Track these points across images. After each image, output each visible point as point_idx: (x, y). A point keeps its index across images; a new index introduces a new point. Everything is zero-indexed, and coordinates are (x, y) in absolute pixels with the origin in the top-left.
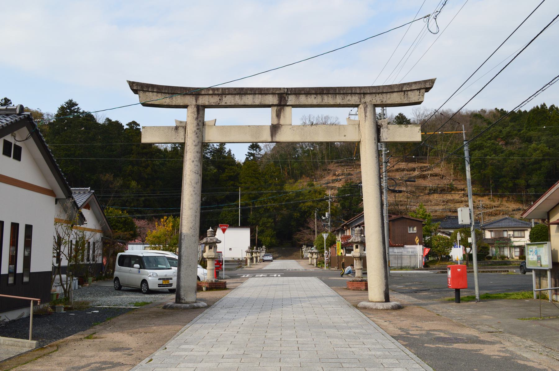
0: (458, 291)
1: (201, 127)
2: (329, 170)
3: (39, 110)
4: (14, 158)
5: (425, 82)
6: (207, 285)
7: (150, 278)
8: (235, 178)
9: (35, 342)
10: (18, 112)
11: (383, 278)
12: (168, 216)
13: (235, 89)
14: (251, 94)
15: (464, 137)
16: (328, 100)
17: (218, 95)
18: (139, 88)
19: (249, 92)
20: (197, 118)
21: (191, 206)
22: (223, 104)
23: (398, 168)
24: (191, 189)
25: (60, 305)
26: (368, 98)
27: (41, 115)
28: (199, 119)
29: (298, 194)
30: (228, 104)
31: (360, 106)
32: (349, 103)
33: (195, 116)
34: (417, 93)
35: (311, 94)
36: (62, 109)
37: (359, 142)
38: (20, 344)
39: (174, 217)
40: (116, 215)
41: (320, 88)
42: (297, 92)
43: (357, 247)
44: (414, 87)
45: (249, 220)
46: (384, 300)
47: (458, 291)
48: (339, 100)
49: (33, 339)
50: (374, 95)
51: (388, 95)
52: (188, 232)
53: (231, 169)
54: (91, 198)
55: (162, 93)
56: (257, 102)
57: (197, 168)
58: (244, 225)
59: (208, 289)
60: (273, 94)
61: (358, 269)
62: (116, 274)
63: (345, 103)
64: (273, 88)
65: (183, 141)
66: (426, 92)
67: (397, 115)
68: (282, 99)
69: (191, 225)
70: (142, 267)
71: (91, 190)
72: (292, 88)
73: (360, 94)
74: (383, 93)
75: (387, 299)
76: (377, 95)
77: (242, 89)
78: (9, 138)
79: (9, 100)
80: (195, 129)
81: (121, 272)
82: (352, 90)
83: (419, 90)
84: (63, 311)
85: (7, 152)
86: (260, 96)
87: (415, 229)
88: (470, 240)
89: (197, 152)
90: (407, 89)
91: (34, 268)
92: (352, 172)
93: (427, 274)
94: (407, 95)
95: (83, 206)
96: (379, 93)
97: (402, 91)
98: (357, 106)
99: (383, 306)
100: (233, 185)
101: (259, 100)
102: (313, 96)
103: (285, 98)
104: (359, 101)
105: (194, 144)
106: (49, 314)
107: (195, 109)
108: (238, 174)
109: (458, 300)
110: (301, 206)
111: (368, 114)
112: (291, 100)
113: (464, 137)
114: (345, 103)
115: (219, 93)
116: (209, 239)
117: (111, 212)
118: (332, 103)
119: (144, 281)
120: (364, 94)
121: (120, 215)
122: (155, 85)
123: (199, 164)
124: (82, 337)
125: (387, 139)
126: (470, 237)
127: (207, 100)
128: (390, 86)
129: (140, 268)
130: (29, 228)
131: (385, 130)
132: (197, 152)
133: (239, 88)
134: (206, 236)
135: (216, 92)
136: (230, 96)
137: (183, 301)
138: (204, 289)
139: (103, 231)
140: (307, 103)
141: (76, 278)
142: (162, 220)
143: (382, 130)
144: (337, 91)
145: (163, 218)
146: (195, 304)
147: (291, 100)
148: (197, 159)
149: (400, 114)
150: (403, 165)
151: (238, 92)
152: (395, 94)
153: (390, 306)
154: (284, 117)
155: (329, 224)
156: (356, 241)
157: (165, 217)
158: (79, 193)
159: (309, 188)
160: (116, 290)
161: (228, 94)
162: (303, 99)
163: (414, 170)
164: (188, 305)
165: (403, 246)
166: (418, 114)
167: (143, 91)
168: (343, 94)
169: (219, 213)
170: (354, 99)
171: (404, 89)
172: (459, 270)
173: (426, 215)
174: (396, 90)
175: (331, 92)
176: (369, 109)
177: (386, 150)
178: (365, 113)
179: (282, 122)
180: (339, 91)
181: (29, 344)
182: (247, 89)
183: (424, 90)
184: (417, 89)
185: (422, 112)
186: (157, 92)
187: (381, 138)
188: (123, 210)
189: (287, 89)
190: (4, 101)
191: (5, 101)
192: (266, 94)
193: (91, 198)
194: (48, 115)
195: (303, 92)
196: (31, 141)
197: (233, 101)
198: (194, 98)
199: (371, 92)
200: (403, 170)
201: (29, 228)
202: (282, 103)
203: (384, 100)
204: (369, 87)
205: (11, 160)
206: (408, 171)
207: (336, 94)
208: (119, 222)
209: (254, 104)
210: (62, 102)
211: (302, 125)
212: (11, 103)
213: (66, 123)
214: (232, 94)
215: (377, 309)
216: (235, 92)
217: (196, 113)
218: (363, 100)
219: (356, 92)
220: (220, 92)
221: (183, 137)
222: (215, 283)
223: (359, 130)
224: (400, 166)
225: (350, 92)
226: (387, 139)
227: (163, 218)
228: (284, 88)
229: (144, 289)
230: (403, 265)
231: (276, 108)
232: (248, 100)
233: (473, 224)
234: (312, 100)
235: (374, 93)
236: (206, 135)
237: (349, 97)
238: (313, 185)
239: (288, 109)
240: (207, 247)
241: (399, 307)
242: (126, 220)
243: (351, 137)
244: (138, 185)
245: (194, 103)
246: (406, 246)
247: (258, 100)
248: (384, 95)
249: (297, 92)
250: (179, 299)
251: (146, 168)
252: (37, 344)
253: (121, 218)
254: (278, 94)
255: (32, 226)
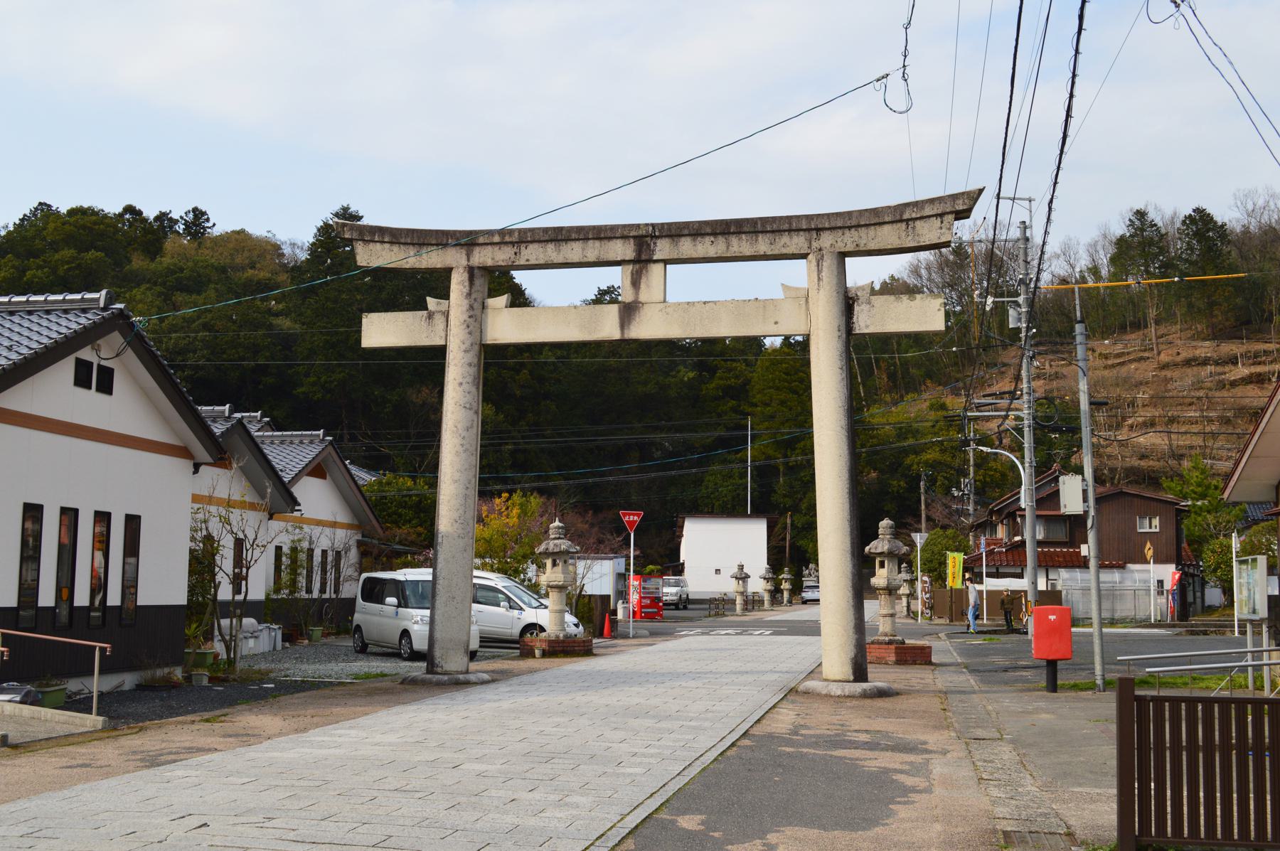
0: (1052, 665)
1: (478, 312)
2: (1005, 365)
3: (270, 235)
4: (98, 390)
5: (954, 197)
6: (545, 646)
7: (416, 627)
8: (739, 392)
9: (101, 718)
10: (102, 305)
11: (851, 631)
12: (511, 492)
13: (546, 230)
14: (578, 240)
15: (1078, 314)
16: (740, 245)
17: (513, 243)
18: (355, 235)
19: (574, 236)
20: (469, 295)
21: (457, 476)
22: (522, 262)
23: (1191, 356)
24: (457, 441)
25: (201, 671)
26: (827, 240)
27: (276, 248)
28: (473, 296)
29: (904, 431)
30: (533, 262)
31: (810, 257)
32: (784, 251)
33: (466, 290)
34: (936, 222)
35: (703, 235)
36: (325, 229)
37: (807, 338)
38: (78, 721)
39: (524, 495)
40: (399, 490)
41: (722, 221)
42: (673, 232)
43: (882, 565)
44: (928, 211)
45: (774, 498)
46: (852, 678)
47: (1052, 665)
48: (763, 245)
49: (99, 714)
50: (840, 232)
51: (872, 231)
52: (450, 530)
53: (730, 370)
54: (324, 454)
55: (399, 243)
56: (591, 257)
57: (469, 398)
58: (757, 513)
59: (545, 654)
60: (624, 237)
61: (885, 616)
62: (358, 618)
63: (777, 250)
64: (624, 226)
65: (442, 343)
66: (956, 219)
67: (1189, 211)
68: (645, 245)
69: (456, 515)
70: (403, 603)
71: (325, 435)
72: (663, 224)
73: (809, 230)
74: (859, 226)
75: (860, 673)
76: (847, 231)
77: (560, 229)
78: (86, 354)
79: (204, 213)
80: (465, 317)
81: (368, 615)
82: (790, 224)
83: (941, 215)
84: (205, 682)
85: (82, 380)
86: (597, 243)
87: (1156, 522)
88: (1084, 550)
89: (470, 365)
90: (914, 215)
91: (146, 597)
92: (1065, 371)
93: (1159, 635)
94: (914, 228)
95: (306, 471)
96: (850, 228)
97: (901, 221)
98: (804, 256)
99: (843, 690)
100: (735, 410)
101: (596, 252)
102: (708, 239)
103: (649, 245)
104: (806, 245)
105: (463, 347)
106: (174, 687)
107: (466, 275)
108: (747, 382)
109: (1053, 687)
110: (908, 461)
111: (825, 274)
112: (663, 249)
113: (1078, 314)
114: (776, 252)
115: (514, 239)
116: (552, 544)
117: (389, 483)
118: (748, 254)
119: (405, 633)
120: (819, 230)
121: (409, 489)
122: (387, 229)
123: (474, 390)
124: (198, 718)
125: (867, 327)
126: (1086, 542)
127: (490, 255)
128: (875, 211)
129: (399, 606)
130: (133, 522)
131: (865, 307)
132: (470, 365)
133: (554, 229)
134: (548, 538)
135: (507, 239)
136: (536, 246)
137: (439, 670)
138: (537, 653)
139: (359, 525)
140: (695, 255)
141: (276, 627)
142: (497, 501)
143: (856, 308)
144: (759, 227)
145: (500, 497)
146: (461, 677)
147: (663, 249)
148: (469, 379)
149: (1197, 210)
150: (1205, 349)
151: (553, 236)
152: (886, 228)
153: (859, 690)
154: (648, 286)
155: (971, 508)
156: (879, 550)
157: (505, 495)
158: (301, 442)
159: (932, 415)
160: (357, 652)
161: (532, 242)
162: (687, 247)
163: (1233, 361)
164: (446, 678)
165: (1122, 567)
166: (1250, 207)
167: (364, 240)
168: (773, 232)
169: (698, 482)
170: (797, 242)
171: (906, 216)
172: (1052, 617)
173: (1208, 487)
174: (887, 219)
175: (746, 229)
176: (829, 263)
177: (1028, 329)
178: (819, 271)
179: (642, 298)
180: (763, 225)
181: (93, 721)
182: (571, 229)
183: (951, 217)
184: (936, 216)
185: (1261, 202)
186: (391, 243)
187: (856, 326)
188: (414, 478)
189: (653, 225)
190: (191, 215)
191: (195, 216)
192: (610, 238)
193: (324, 454)
194: (293, 245)
195: (686, 232)
196: (130, 355)
197: (542, 256)
198: (464, 252)
199: (833, 225)
200: (1205, 362)
201: (133, 522)
202: (644, 257)
203: (862, 242)
204: (828, 215)
205: (91, 396)
206: (1217, 363)
207: (756, 232)
208: (404, 505)
209: (585, 260)
210: (324, 213)
211: (696, 300)
212: (208, 220)
213: (329, 267)
214: (539, 241)
215: (828, 696)
216: (547, 238)
217: (467, 284)
218: (815, 245)
219: (800, 226)
220: (515, 238)
221: (443, 334)
222: (563, 642)
223: (808, 309)
224: (1197, 352)
225: (786, 226)
226: (867, 327)
227: (500, 497)
228: (647, 225)
229: (405, 650)
230: (1117, 615)
231: (630, 267)
232: (574, 251)
233: (1092, 513)
234: (706, 247)
235: (840, 228)
236: (489, 329)
237: (785, 239)
238: (943, 407)
239: (656, 269)
240: (549, 562)
241: (882, 694)
242: (420, 502)
243: (794, 326)
244: (497, 413)
245: (464, 262)
246: (1130, 566)
247: (593, 250)
248: (863, 231)
249: (675, 231)
250: (431, 669)
251: (518, 372)
252: (104, 722)
253: (410, 496)
254: (634, 237)
255: (139, 517)
